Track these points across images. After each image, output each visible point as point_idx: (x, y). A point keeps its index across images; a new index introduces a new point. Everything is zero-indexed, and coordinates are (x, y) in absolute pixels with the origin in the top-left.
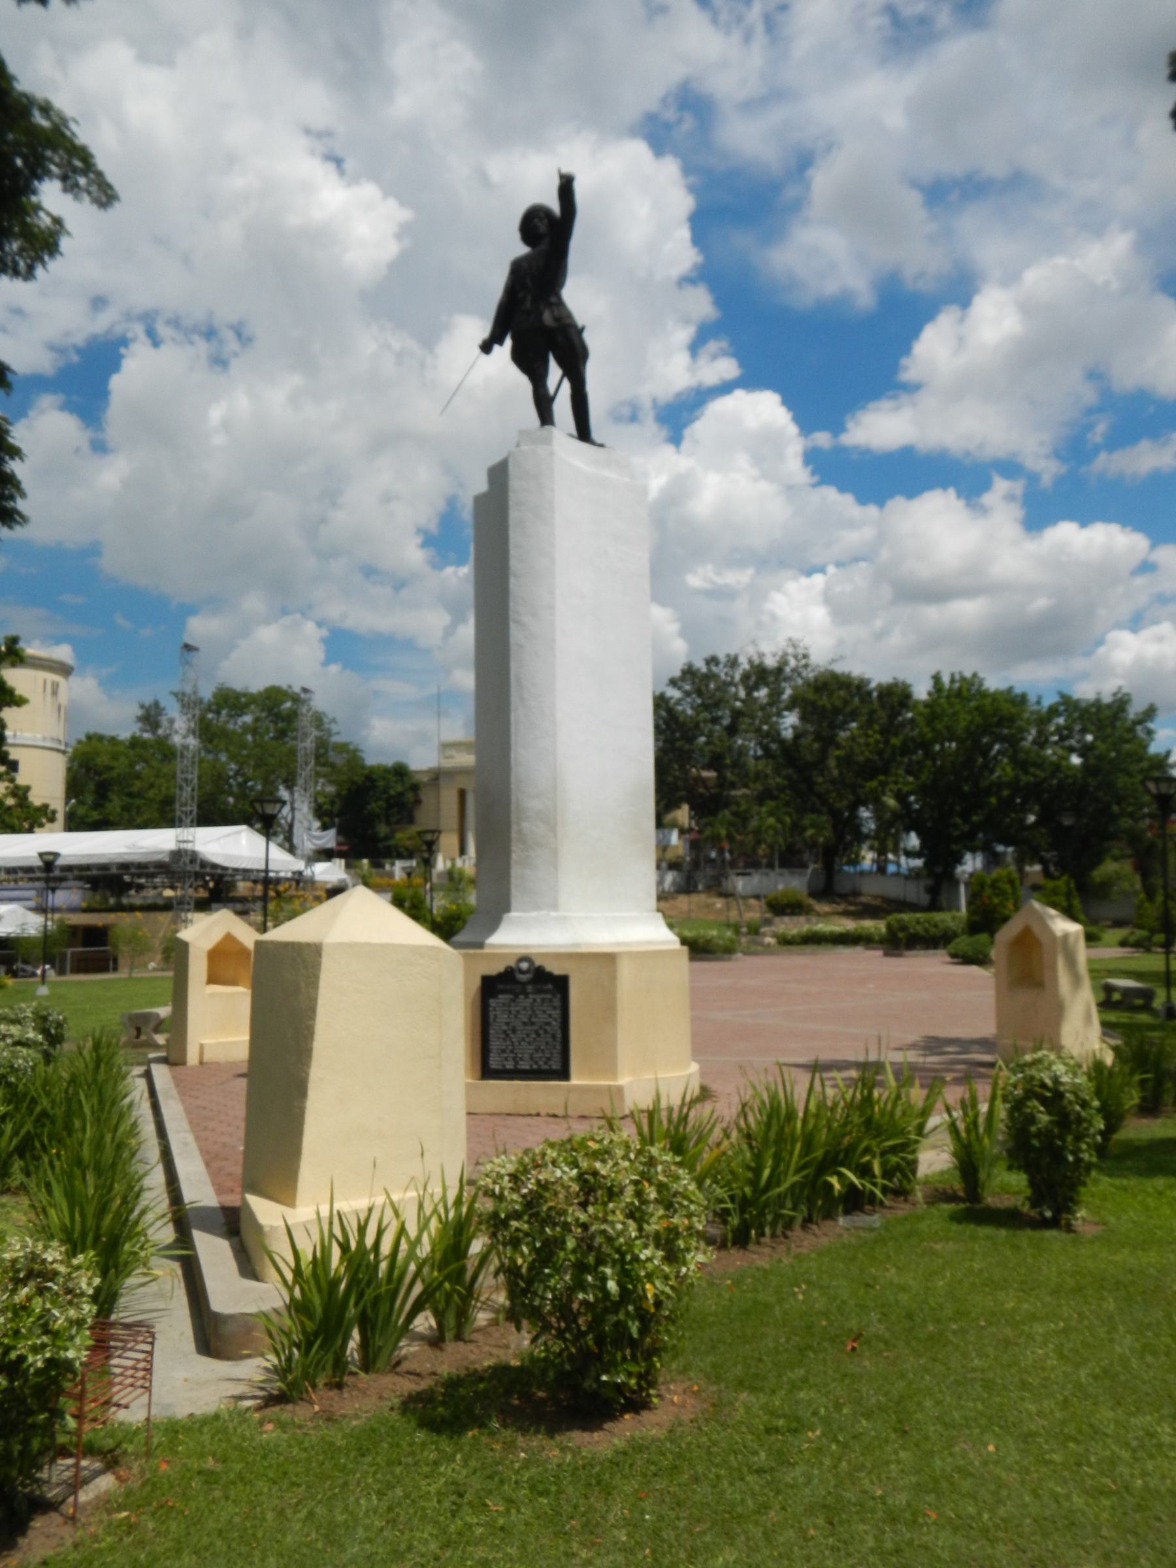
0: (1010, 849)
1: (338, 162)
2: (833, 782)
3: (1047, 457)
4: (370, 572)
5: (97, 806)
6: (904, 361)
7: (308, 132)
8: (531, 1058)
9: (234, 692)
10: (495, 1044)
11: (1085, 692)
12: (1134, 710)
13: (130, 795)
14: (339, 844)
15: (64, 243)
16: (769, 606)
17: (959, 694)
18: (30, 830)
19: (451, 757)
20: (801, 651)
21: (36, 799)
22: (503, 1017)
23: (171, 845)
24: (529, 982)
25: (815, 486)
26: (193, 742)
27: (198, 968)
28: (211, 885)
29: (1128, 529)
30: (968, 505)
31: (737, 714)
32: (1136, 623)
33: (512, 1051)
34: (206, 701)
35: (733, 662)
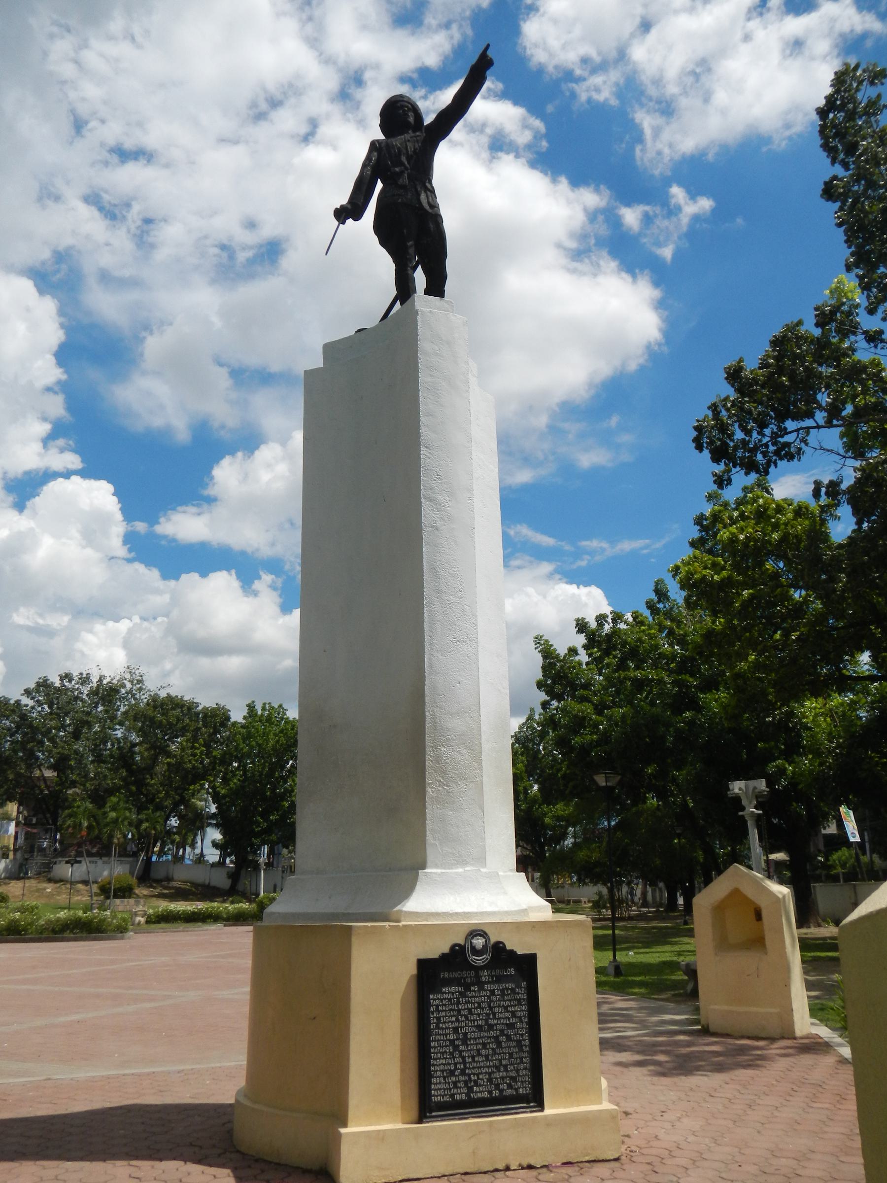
8: (490, 1080)
10: (438, 1064)
16: (79, 645)
17: (269, 719)
22: (449, 1021)
24: (482, 968)
25: (129, 561)
30: (242, 587)
33: (463, 1072)
35: (85, 680)
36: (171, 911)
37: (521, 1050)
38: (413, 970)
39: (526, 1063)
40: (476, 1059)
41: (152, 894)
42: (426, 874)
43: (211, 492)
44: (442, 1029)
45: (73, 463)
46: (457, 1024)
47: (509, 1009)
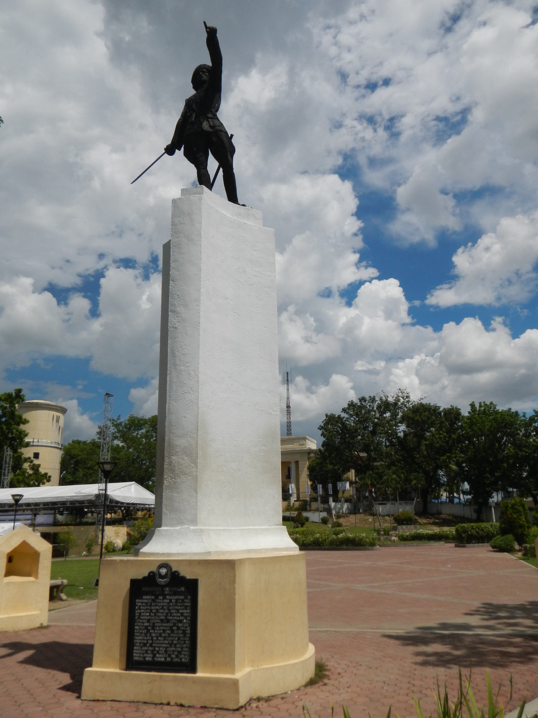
0: (515, 490)
8: (166, 651)
9: (137, 418)
10: (138, 639)
17: (484, 412)
18: (38, 486)
20: (405, 395)
21: (42, 470)
22: (146, 615)
23: (96, 492)
24: (167, 585)
25: (413, 325)
31: (375, 425)
33: (151, 645)
35: (373, 400)
36: (419, 534)
38: (127, 586)
39: (187, 644)
40: (159, 638)
41: (429, 522)
42: (159, 531)
44: (142, 619)
45: (373, 273)
46: (149, 617)
47: (180, 611)
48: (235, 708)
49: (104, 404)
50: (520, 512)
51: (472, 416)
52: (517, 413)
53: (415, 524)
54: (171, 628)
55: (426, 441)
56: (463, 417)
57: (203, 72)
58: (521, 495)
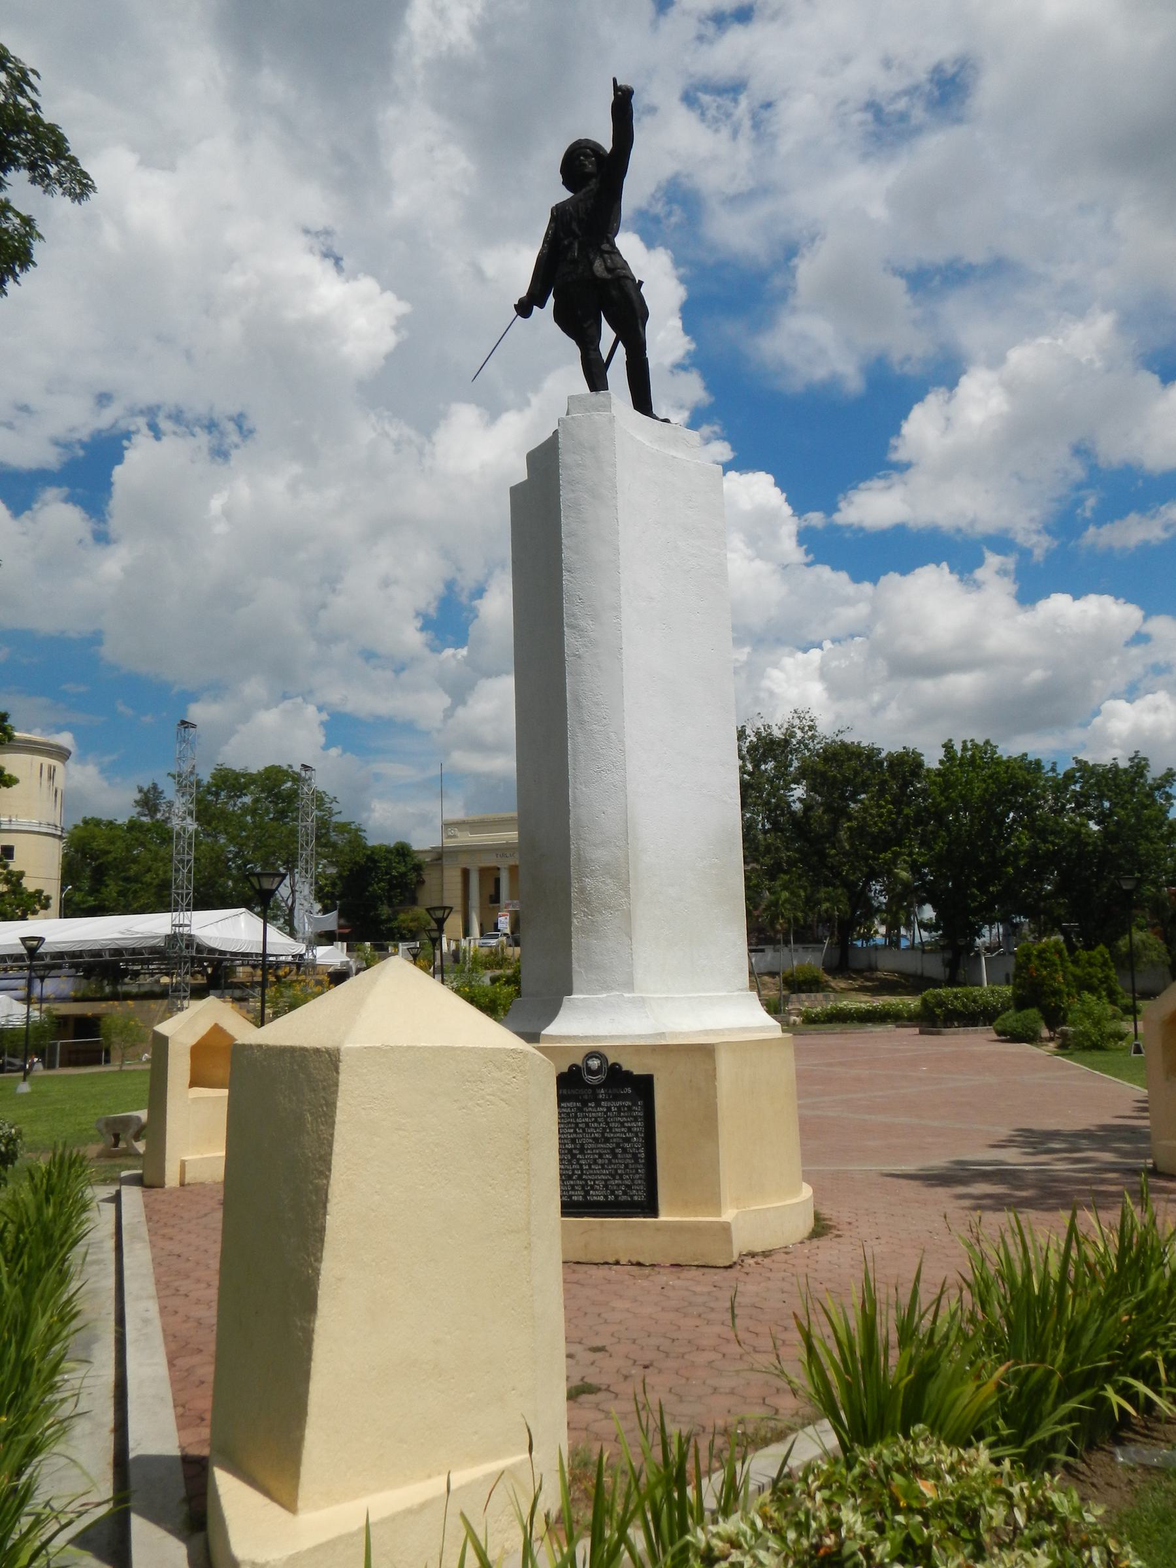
1: (337, 261)
2: (846, 854)
3: (1039, 532)
4: (369, 656)
5: (93, 891)
6: (893, 441)
7: (307, 232)
8: (606, 1186)
11: (1101, 757)
12: (1155, 772)
13: (127, 879)
14: (340, 927)
15: (38, 250)
18: (23, 918)
19: (454, 836)
21: (29, 885)
23: (168, 930)
24: (600, 1086)
25: (808, 565)
26: (192, 825)
27: (179, 1067)
28: (210, 970)
29: (1122, 600)
30: (961, 580)
32: (1131, 693)
33: (580, 1177)
34: (205, 783)
37: (636, 1162)
41: (852, 987)
43: (900, 455)
46: (575, 1135)
47: (626, 1124)
48: (727, 1264)
49: (178, 745)
50: (1055, 965)
51: (948, 769)
52: (1038, 763)
53: (823, 991)
54: (612, 1150)
55: (849, 820)
56: (928, 770)
57: (587, 156)
58: (1041, 932)
